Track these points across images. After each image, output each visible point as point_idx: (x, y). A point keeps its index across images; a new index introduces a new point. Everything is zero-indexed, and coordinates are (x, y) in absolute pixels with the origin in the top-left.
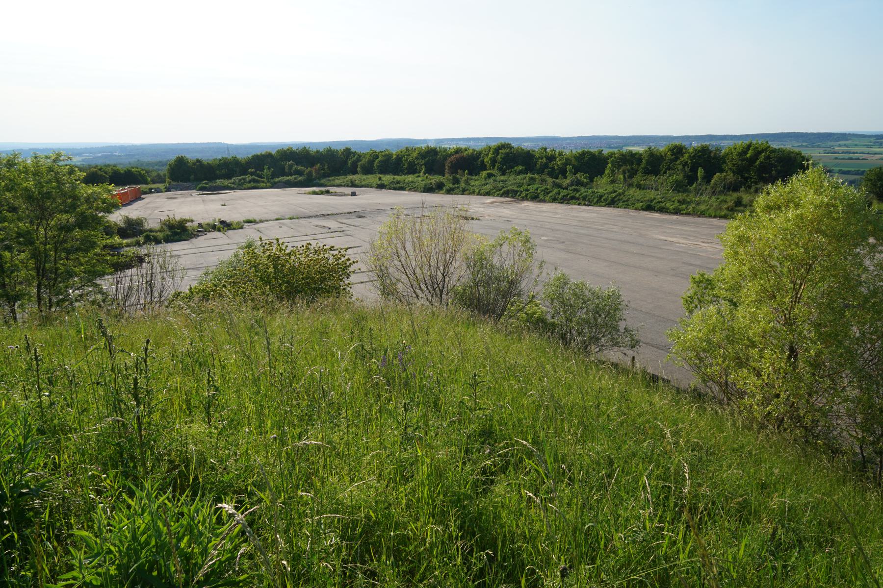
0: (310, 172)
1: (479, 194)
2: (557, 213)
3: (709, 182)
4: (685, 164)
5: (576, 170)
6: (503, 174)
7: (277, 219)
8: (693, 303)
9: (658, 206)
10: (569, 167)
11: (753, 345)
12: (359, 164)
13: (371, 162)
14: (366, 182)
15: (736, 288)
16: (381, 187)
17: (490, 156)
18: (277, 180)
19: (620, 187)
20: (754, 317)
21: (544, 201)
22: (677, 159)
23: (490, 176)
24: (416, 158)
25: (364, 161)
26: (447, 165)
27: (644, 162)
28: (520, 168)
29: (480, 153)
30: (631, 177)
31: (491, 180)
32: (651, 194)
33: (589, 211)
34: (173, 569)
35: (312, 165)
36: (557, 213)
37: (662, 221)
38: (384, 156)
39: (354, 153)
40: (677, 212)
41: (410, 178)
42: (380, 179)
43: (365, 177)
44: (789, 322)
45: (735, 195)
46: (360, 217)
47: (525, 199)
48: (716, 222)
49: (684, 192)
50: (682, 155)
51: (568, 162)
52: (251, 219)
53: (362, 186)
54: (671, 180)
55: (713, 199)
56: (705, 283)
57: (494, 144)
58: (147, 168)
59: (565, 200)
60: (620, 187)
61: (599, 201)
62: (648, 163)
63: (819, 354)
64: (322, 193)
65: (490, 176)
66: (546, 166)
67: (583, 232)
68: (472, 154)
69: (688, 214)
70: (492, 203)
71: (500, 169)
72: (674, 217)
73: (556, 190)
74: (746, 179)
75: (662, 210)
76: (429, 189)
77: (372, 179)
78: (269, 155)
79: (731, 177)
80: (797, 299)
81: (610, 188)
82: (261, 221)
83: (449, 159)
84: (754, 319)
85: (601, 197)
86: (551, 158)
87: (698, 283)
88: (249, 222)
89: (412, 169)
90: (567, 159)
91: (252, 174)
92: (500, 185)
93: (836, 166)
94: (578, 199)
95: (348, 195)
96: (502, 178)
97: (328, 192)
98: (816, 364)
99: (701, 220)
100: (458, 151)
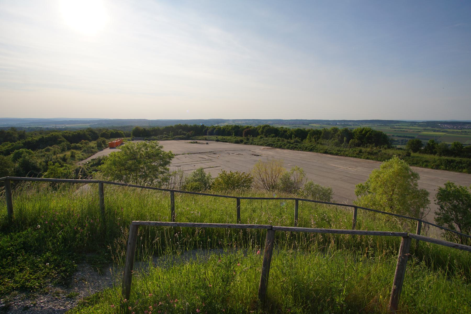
1: (258, 145)
3: (348, 142)
4: (339, 135)
5: (296, 136)
6: (266, 137)
10: (293, 135)
13: (213, 131)
16: (218, 141)
17: (261, 130)
21: (284, 149)
22: (335, 133)
23: (261, 138)
24: (231, 130)
26: (244, 133)
28: (273, 135)
29: (257, 128)
30: (317, 140)
39: (205, 127)
40: (337, 154)
41: (229, 137)
43: (210, 136)
45: (359, 148)
46: (215, 154)
47: (276, 147)
48: (352, 159)
49: (339, 146)
51: (292, 133)
55: (351, 150)
59: (293, 148)
61: (306, 149)
64: (194, 143)
65: (261, 138)
69: (341, 155)
70: (264, 149)
71: (265, 135)
72: (336, 157)
73: (288, 144)
74: (362, 142)
75: (331, 154)
76: (237, 142)
77: (214, 137)
79: (357, 141)
81: (310, 144)
82: (177, 155)
85: (307, 148)
86: (285, 131)
87: (360, 187)
89: (229, 134)
90: (292, 132)
91: (165, 134)
92: (266, 141)
96: (266, 139)
97: (196, 142)
100: (248, 127)
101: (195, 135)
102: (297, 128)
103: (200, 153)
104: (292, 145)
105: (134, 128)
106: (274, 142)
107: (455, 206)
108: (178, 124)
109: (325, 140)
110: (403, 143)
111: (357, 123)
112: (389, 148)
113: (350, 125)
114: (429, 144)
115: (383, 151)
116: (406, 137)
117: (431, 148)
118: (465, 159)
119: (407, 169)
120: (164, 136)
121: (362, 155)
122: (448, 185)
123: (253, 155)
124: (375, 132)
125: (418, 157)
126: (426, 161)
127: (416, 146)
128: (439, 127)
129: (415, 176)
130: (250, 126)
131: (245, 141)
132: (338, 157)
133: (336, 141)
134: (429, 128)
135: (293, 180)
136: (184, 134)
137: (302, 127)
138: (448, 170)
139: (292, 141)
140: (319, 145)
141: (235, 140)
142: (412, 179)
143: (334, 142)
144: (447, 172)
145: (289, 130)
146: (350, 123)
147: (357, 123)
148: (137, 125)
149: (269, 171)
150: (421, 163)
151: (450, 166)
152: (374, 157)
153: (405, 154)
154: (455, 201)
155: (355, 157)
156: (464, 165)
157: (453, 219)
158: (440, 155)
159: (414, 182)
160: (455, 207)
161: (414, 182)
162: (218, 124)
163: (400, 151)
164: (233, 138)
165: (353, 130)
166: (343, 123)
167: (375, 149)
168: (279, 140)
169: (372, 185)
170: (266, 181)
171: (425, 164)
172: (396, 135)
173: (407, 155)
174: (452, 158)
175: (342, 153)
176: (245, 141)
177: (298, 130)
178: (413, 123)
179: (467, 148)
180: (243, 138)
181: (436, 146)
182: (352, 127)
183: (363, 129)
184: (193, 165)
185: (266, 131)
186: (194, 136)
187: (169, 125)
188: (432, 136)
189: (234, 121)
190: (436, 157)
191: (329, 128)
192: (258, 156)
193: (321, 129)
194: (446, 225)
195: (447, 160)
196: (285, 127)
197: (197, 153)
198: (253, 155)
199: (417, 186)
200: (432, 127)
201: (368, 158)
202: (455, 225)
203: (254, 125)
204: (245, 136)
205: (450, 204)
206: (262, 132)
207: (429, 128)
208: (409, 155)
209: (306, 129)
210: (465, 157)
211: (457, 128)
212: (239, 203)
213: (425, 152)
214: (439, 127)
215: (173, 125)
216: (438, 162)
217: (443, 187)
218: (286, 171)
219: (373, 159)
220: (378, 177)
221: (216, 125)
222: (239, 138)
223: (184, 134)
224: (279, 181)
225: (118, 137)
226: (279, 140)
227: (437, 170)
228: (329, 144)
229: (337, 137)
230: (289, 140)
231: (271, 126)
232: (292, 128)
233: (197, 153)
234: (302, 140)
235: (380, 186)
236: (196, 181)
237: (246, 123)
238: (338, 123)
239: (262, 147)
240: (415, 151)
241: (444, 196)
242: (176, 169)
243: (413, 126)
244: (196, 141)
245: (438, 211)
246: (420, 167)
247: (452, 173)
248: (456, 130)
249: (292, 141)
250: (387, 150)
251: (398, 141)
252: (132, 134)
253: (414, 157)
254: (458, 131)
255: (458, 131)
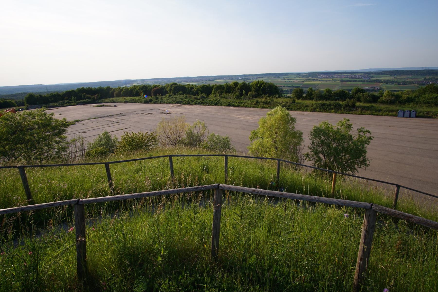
0: (94, 98)
1: (167, 103)
2: (198, 109)
3: (247, 95)
4: (239, 89)
5: (202, 92)
6: (175, 95)
7: (89, 119)
8: (252, 139)
9: (232, 104)
10: (199, 92)
11: (268, 148)
12: (115, 93)
13: (120, 92)
14: (119, 100)
15: (263, 134)
16: (126, 102)
17: (169, 88)
18: (79, 101)
19: (218, 98)
20: (268, 141)
21: (192, 105)
22: (236, 87)
23: (170, 96)
24: (139, 90)
25: (116, 92)
26: (152, 92)
27: (225, 89)
28: (181, 92)
29: (165, 87)
30: (221, 94)
31: (171, 97)
32: (229, 100)
33: (209, 108)
34: (31, 278)
35: (94, 95)
36: (198, 109)
37: (234, 110)
38: (125, 89)
39: (111, 89)
40: (238, 106)
41: (137, 98)
42: (125, 99)
43: (118, 98)
44: (275, 142)
45: (256, 99)
46: (123, 116)
47: (185, 104)
48: (251, 109)
49: (240, 99)
50: (238, 86)
51: (198, 90)
52: (77, 120)
53: (118, 102)
54: (235, 95)
55: (249, 101)
56: (255, 133)
57: (170, 83)
58: (5, 98)
59: (200, 104)
60: (218, 98)
61: (211, 104)
62: (227, 89)
63: (282, 148)
64: (101, 106)
65: (170, 96)
66: (190, 91)
67: (209, 116)
68: (162, 87)
69: (242, 107)
70: (173, 106)
71: (173, 93)
72: (238, 108)
73: (196, 100)
74: (259, 93)
75: (234, 106)
76: (146, 102)
77: (121, 99)
78: (73, 91)
79: (254, 93)
80: (277, 136)
81: (215, 99)
82: (82, 120)
83: (153, 90)
84: (268, 142)
85: (212, 102)
86: (192, 88)
87: (253, 133)
88: (77, 121)
89: (138, 94)
90: (198, 88)
91: (67, 99)
92: (175, 99)
93: (286, 84)
94: (204, 103)
95: (113, 106)
96: (175, 96)
97: (104, 106)
98: (281, 151)
99: (246, 109)
100: (155, 87)
101: (101, 98)
102: (202, 84)
103: (108, 116)
104: (199, 101)
105: (27, 96)
106: (182, 99)
108: (80, 87)
109: (228, 94)
110: (291, 92)
111: (255, 77)
112: (279, 97)
114: (308, 92)
115: (275, 100)
116: (294, 87)
117: (310, 96)
118: (333, 102)
120: (66, 101)
121: (258, 105)
123: (162, 113)
124: (268, 84)
125: (301, 103)
127: (299, 93)
128: (317, 77)
129: (293, 120)
130: (158, 85)
131: (154, 100)
133: (237, 94)
136: (89, 98)
138: (322, 112)
140: (223, 99)
142: (291, 123)
143: (235, 95)
144: (321, 114)
145: (196, 86)
147: (255, 77)
148: (31, 91)
149: (173, 127)
150: (303, 108)
151: (324, 108)
152: (268, 106)
153: (291, 101)
154: (323, 137)
155: (253, 107)
156: (332, 107)
158: (316, 100)
160: (322, 142)
163: (288, 99)
165: (251, 84)
166: (244, 78)
167: (269, 99)
168: (186, 96)
170: (171, 138)
172: (286, 85)
173: (292, 102)
174: (324, 102)
175: (242, 104)
176: (154, 100)
177: (204, 86)
178: (298, 75)
179: (334, 93)
182: (252, 80)
183: (258, 82)
184: (101, 129)
187: (70, 89)
188: (312, 85)
189: (142, 81)
190: (313, 102)
191: (231, 82)
193: (224, 84)
195: (321, 103)
197: (105, 117)
198: (162, 113)
201: (263, 108)
202: (321, 155)
203: (163, 84)
204: (154, 95)
207: (310, 78)
208: (294, 102)
209: (211, 85)
211: (329, 78)
212: (108, 169)
213: (305, 98)
214: (317, 77)
215: (75, 89)
216: (315, 106)
218: (189, 125)
219: (267, 108)
221: (124, 86)
225: (8, 107)
227: (314, 113)
228: (232, 97)
230: (196, 97)
231: (178, 84)
233: (105, 117)
234: (208, 95)
236: (102, 145)
237: (155, 82)
238: (239, 78)
239: (171, 105)
240: (298, 98)
241: (317, 133)
242: (75, 136)
243: (298, 77)
246: (302, 111)
247: (324, 114)
248: (328, 79)
250: (278, 99)
251: (287, 91)
252: (25, 102)
253: (298, 103)
254: (330, 79)
255: (330, 79)
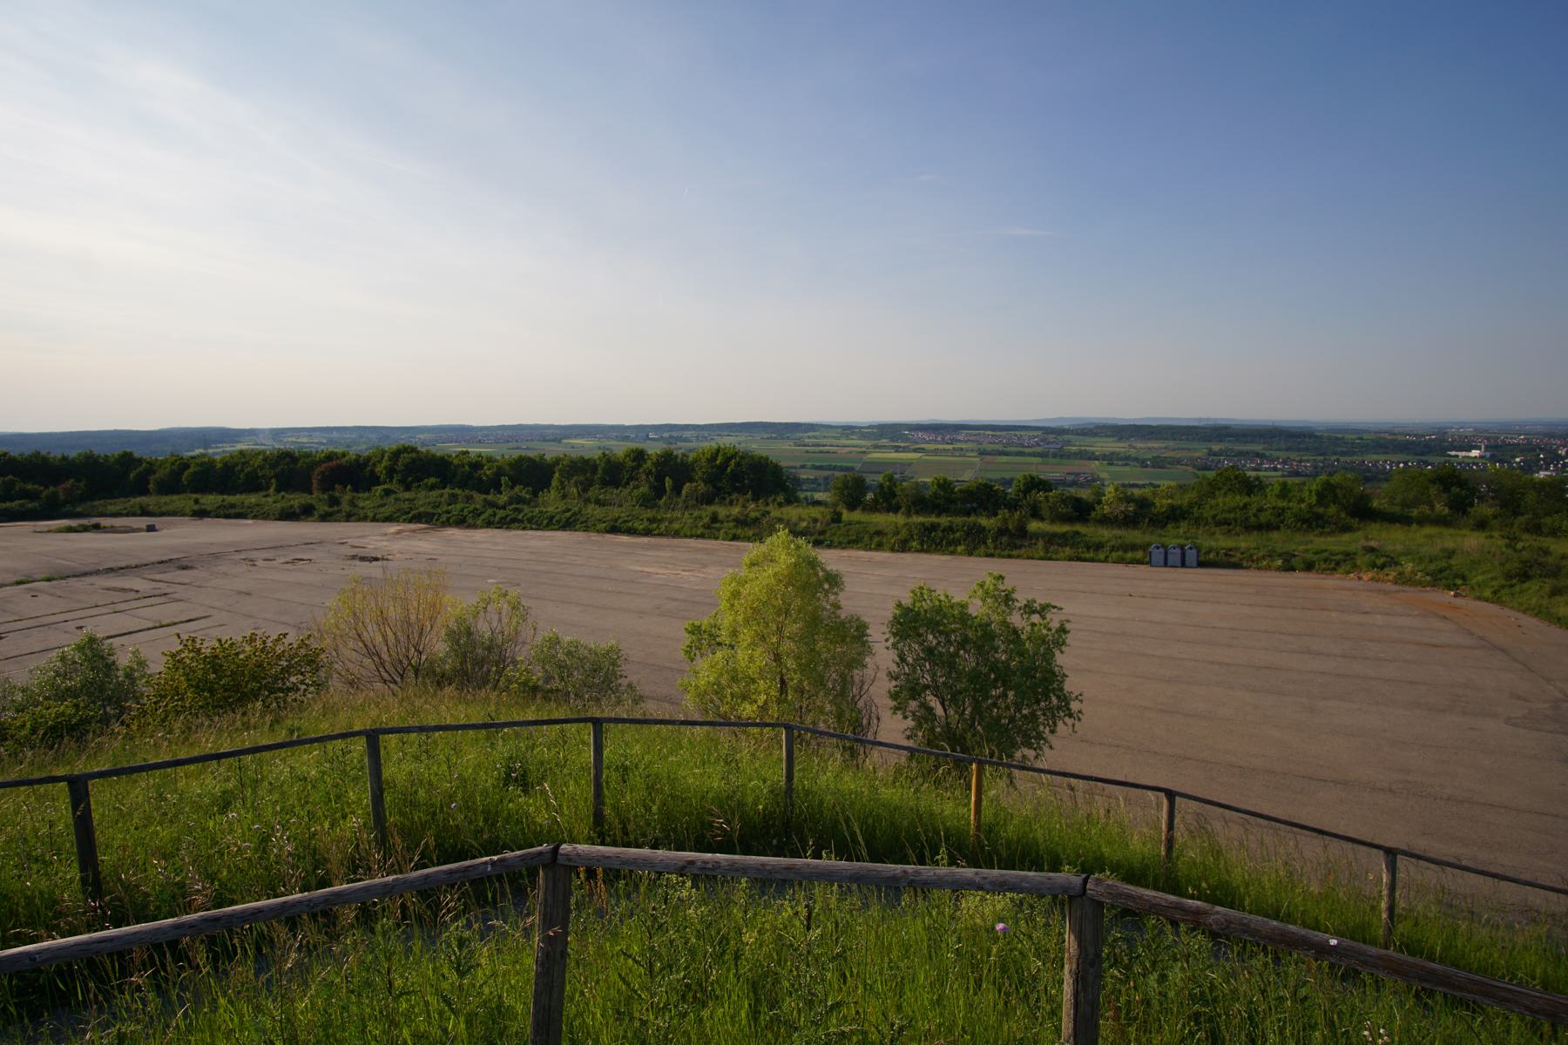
1: (374, 520)
5: (514, 482)
6: (408, 489)
10: (504, 479)
16: (201, 514)
21: (474, 526)
22: (639, 466)
28: (432, 480)
29: (369, 459)
39: (140, 461)
41: (253, 499)
43: (165, 499)
45: (711, 509)
46: (184, 568)
48: (692, 542)
49: (652, 507)
51: (500, 472)
55: (687, 515)
59: (505, 524)
64: (85, 529)
65: (388, 493)
69: (661, 535)
70: (399, 532)
71: (400, 481)
72: (646, 540)
73: (490, 511)
74: (719, 489)
75: (631, 532)
76: (288, 515)
77: (177, 501)
79: (702, 488)
81: (562, 506)
85: (552, 518)
86: (476, 466)
89: (254, 484)
90: (499, 468)
92: (406, 505)
96: (407, 495)
97: (97, 527)
100: (330, 457)
102: (516, 454)
103: (111, 570)
104: (501, 513)
107: (930, 651)
110: (825, 484)
112: (789, 502)
113: (686, 440)
116: (835, 468)
117: (888, 499)
118: (959, 520)
119: (813, 564)
122: (919, 595)
123: (354, 557)
124: (752, 457)
126: (879, 533)
127: (854, 492)
128: (907, 439)
129: (834, 580)
130: (340, 450)
131: (324, 508)
132: (652, 540)
134: (884, 442)
135: (488, 635)
136: (33, 496)
137: (534, 450)
138: (927, 551)
139: (503, 499)
140: (591, 506)
141: (279, 505)
144: (924, 558)
146: (687, 434)
149: (394, 613)
150: (866, 538)
151: (932, 541)
155: (702, 536)
157: (927, 687)
159: (832, 597)
161: (832, 597)
162: (206, 447)
164: (271, 499)
166: (666, 435)
167: (753, 510)
169: (726, 621)
170: (385, 657)
171: (876, 539)
173: (833, 521)
174: (933, 519)
175: (663, 526)
176: (324, 508)
177: (521, 459)
178: (848, 430)
180: (316, 498)
181: (898, 491)
183: (718, 450)
184: (72, 625)
185: (406, 466)
186: (84, 499)
188: (892, 464)
189: (277, 433)
190: (899, 519)
191: (620, 449)
192: (376, 559)
194: (913, 704)
195: (923, 524)
196: (474, 450)
197: (97, 572)
198: (354, 557)
199: (839, 608)
200: (892, 440)
201: (735, 538)
202: (934, 703)
204: (324, 490)
205: (921, 644)
206: (391, 471)
207: (884, 442)
208: (837, 518)
210: (957, 513)
211: (943, 442)
213: (873, 508)
214: (907, 439)
216: (904, 534)
217: (907, 601)
218: (457, 604)
220: (736, 595)
221: (198, 452)
222: (297, 500)
223: (33, 496)
224: (439, 647)
226: (454, 496)
228: (624, 502)
229: (643, 477)
230: (490, 497)
232: (502, 452)
234: (535, 494)
235: (747, 621)
236: (61, 696)
237: (331, 441)
239: (393, 528)
240: (852, 507)
241: (908, 623)
243: (847, 437)
244: (95, 520)
245: (894, 668)
249: (503, 499)
250: (784, 510)
251: (815, 481)
